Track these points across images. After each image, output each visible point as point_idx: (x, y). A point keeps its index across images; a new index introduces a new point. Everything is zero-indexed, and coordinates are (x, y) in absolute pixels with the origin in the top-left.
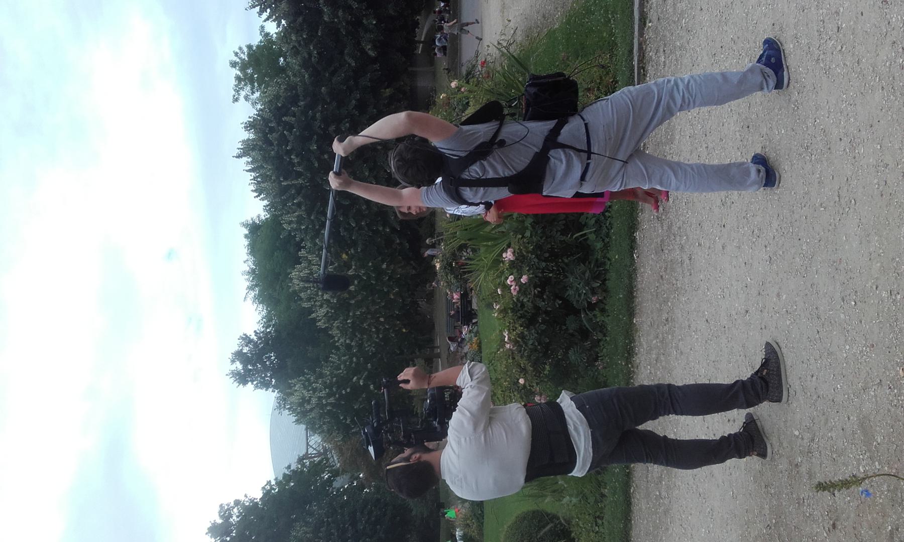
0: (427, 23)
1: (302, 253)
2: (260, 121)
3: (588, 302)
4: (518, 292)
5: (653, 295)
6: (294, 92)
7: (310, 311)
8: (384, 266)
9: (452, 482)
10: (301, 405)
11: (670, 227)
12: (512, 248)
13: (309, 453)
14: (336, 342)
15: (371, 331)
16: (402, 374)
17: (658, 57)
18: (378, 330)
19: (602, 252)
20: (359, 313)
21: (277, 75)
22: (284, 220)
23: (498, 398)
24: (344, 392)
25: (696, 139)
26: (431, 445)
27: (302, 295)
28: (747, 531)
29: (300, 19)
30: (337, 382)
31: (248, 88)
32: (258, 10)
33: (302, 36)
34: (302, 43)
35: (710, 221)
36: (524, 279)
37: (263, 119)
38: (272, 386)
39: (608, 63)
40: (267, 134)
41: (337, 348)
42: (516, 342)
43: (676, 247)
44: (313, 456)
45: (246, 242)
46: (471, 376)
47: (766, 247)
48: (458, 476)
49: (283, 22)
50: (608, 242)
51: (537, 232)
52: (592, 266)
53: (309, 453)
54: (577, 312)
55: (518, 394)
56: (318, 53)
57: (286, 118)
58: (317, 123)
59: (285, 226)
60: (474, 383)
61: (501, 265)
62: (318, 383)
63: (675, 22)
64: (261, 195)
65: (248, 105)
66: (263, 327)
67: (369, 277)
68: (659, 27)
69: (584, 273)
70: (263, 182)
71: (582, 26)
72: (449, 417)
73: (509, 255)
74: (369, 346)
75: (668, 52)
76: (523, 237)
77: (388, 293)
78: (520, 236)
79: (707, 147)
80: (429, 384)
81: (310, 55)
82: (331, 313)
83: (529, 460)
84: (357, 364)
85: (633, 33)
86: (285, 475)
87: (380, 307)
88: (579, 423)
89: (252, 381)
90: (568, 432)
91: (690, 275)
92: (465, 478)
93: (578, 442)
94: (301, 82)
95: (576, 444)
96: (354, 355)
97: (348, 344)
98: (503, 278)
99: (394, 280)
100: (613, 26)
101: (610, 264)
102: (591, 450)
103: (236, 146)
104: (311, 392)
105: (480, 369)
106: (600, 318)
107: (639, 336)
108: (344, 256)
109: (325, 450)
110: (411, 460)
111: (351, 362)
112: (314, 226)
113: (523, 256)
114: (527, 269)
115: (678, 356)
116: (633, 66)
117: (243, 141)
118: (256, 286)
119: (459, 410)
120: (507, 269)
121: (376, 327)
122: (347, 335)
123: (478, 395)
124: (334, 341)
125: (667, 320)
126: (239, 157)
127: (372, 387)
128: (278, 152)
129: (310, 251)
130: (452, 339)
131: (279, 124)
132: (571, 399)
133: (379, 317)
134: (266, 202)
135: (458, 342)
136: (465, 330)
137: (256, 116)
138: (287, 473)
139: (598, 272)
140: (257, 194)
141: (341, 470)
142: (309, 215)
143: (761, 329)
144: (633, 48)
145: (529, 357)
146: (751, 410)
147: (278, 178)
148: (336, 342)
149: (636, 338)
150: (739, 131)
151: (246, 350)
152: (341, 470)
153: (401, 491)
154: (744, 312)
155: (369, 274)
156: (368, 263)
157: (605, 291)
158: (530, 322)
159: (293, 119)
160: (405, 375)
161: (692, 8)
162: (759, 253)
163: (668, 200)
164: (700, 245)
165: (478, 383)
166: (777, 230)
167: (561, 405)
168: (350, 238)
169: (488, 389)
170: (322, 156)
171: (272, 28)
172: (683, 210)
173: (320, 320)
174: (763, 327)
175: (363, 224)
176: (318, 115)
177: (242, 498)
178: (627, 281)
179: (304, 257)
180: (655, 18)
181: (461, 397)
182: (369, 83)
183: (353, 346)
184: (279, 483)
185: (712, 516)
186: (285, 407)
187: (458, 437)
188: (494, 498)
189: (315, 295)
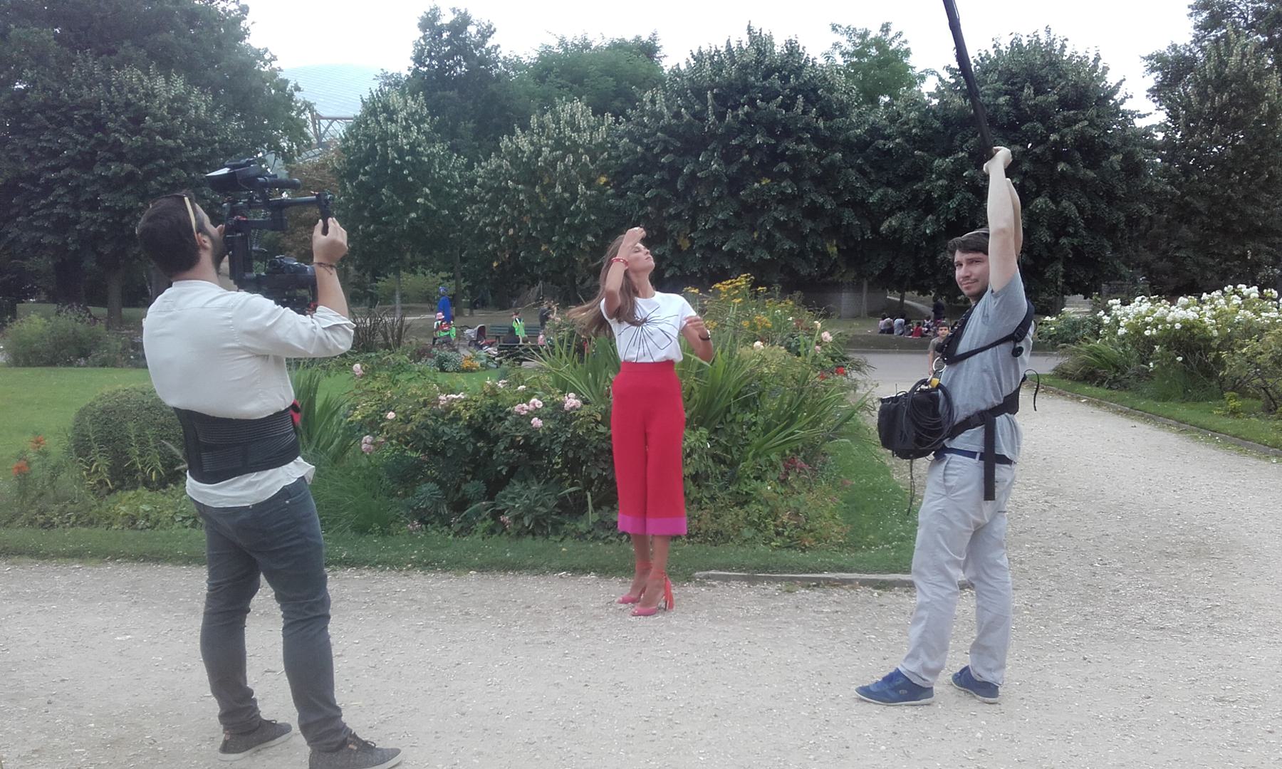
0: (926, 307)
1: (609, 118)
2: (799, 63)
3: (504, 510)
4: (518, 414)
5: (504, 595)
6: (838, 113)
7: (525, 127)
8: (590, 238)
9: (165, 297)
10: (386, 108)
11: (596, 617)
12: (582, 406)
13: (321, 121)
14: (479, 162)
15: (495, 215)
16: (338, 224)
17: (830, 605)
18: (497, 225)
19: (573, 530)
20: (521, 198)
21: (863, 90)
22: (656, 93)
23: (369, 383)
24: (406, 172)
25: (710, 650)
26: (225, 265)
27: (548, 116)
28: (152, 714)
29: (937, 124)
30: (423, 163)
31: (851, 49)
32: (952, 66)
33: (914, 127)
34: (906, 127)
35: (596, 668)
36: (537, 422)
37: (801, 68)
38: (418, 68)
39: (831, 541)
40: (780, 72)
41: (470, 167)
42: (448, 409)
43: (567, 625)
44: (317, 126)
45: (629, 38)
46: (330, 328)
47: (549, 738)
48: (174, 306)
49: (935, 102)
50: (586, 539)
51: (603, 441)
52: (555, 517)
53: (321, 121)
54: (490, 495)
55: (374, 411)
56: (890, 150)
57: (801, 100)
58: (792, 145)
59: (649, 94)
60: (320, 332)
61: (558, 391)
62: (418, 134)
63: (874, 625)
64: (695, 60)
65: (827, 47)
66: (505, 57)
67: (573, 215)
68: (870, 606)
69: (543, 505)
70: (712, 63)
71: (888, 509)
72: (268, 295)
73: (571, 401)
74: (473, 211)
75: (835, 616)
76: (597, 422)
77: (550, 242)
78: (599, 419)
79: (697, 664)
80: (320, 264)
81: (888, 138)
82: (523, 157)
83: (192, 412)
84: (448, 194)
85: (866, 572)
86: (286, 82)
87: (529, 229)
88: (260, 489)
89: (424, 38)
90: (247, 473)
91: (526, 643)
92: (172, 318)
93: (231, 487)
94: (850, 124)
95: (228, 484)
96: (461, 189)
97: (476, 181)
98: (540, 393)
99: (568, 252)
100: (881, 547)
101: (556, 542)
102: (221, 505)
103: (764, 26)
104: (404, 123)
105: (344, 343)
106: (481, 526)
107: (449, 578)
108: (603, 180)
109: (325, 146)
110: (200, 234)
111: (450, 186)
112: (647, 136)
113: (568, 423)
114: (551, 427)
115: (415, 628)
116: (821, 572)
117: (771, 37)
118: (566, 49)
119: (276, 310)
120: (552, 399)
121: (499, 222)
122: (489, 179)
123: (300, 338)
124: (481, 161)
125: (467, 613)
126: (750, 29)
127: (413, 215)
128: (753, 86)
129: (612, 129)
130: (481, 331)
131: (792, 89)
132: (303, 478)
133: (514, 227)
134: (683, 67)
135: (477, 341)
136: (493, 351)
137: (805, 57)
138: (289, 86)
139: (545, 524)
140: (695, 54)
141: (292, 165)
142: (663, 129)
143: (437, 732)
144: (846, 572)
145: (426, 427)
146: (296, 728)
147: (718, 85)
148: (479, 162)
149: (448, 574)
150: (713, 704)
151: (472, 30)
152: (292, 165)
153: (150, 219)
154: (464, 710)
155: (579, 215)
156: (594, 215)
157: (519, 534)
158: (479, 430)
159: (800, 111)
160: (335, 228)
161: (889, 647)
162: (542, 729)
163: (634, 615)
164: (565, 655)
165: (320, 339)
166: (569, 752)
167: (292, 463)
168: (629, 189)
169: (311, 352)
170: (745, 151)
171: (929, 86)
172: (617, 634)
173: (511, 140)
174: (438, 735)
175: (649, 208)
176: (804, 147)
177: (250, 18)
178: (529, 562)
179: (603, 121)
180: (883, 600)
181: (299, 313)
182: (845, 223)
183: (473, 188)
184: (273, 73)
185: (180, 670)
186: (385, 84)
187: (233, 307)
188: (149, 365)
189: (548, 134)
